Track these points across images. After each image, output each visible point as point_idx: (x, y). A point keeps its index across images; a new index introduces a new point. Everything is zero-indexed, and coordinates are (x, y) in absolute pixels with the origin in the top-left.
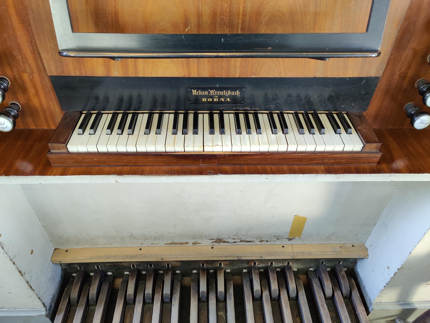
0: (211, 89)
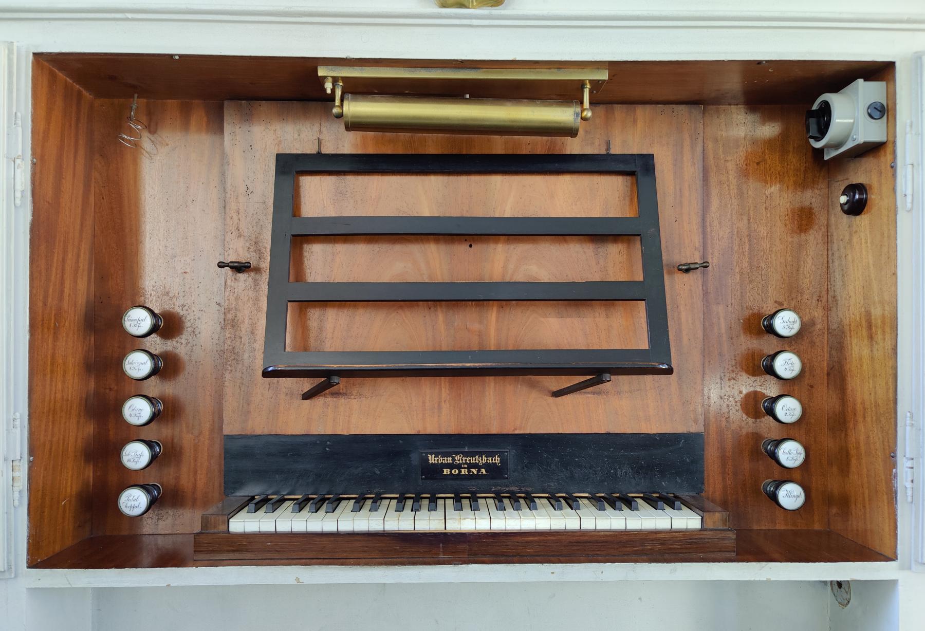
0: (457, 454)
